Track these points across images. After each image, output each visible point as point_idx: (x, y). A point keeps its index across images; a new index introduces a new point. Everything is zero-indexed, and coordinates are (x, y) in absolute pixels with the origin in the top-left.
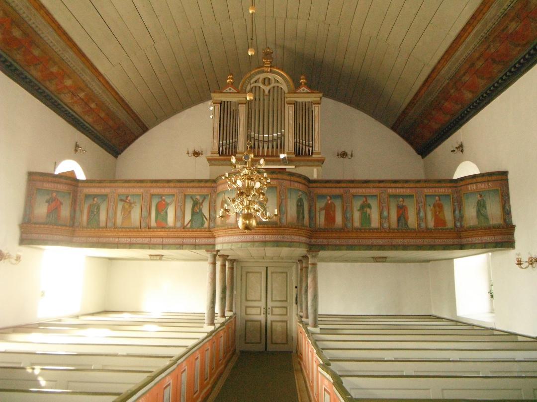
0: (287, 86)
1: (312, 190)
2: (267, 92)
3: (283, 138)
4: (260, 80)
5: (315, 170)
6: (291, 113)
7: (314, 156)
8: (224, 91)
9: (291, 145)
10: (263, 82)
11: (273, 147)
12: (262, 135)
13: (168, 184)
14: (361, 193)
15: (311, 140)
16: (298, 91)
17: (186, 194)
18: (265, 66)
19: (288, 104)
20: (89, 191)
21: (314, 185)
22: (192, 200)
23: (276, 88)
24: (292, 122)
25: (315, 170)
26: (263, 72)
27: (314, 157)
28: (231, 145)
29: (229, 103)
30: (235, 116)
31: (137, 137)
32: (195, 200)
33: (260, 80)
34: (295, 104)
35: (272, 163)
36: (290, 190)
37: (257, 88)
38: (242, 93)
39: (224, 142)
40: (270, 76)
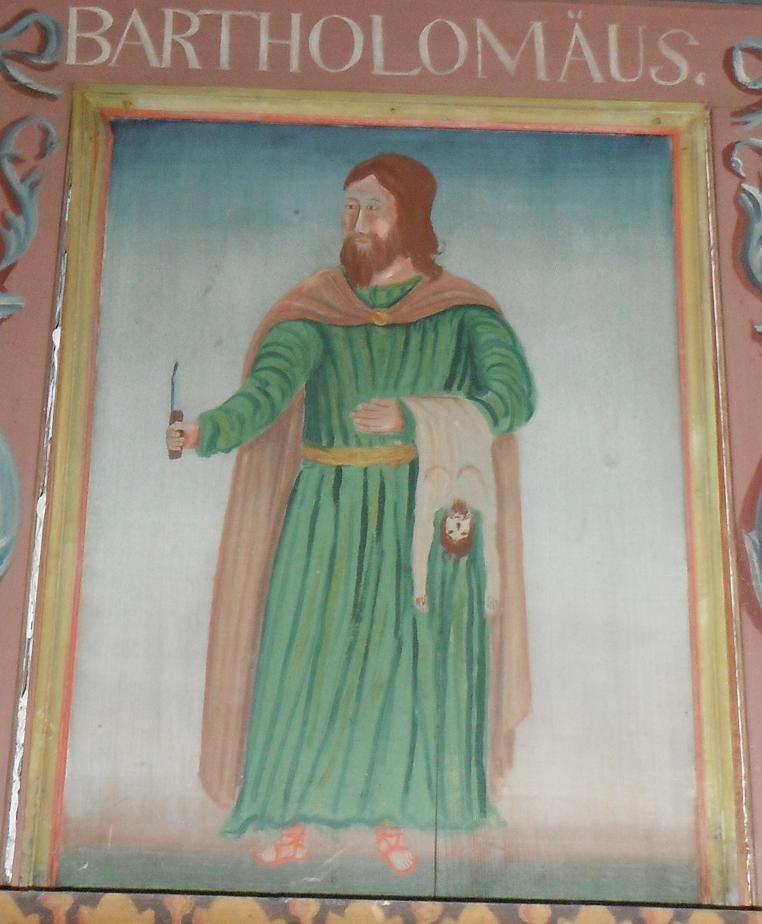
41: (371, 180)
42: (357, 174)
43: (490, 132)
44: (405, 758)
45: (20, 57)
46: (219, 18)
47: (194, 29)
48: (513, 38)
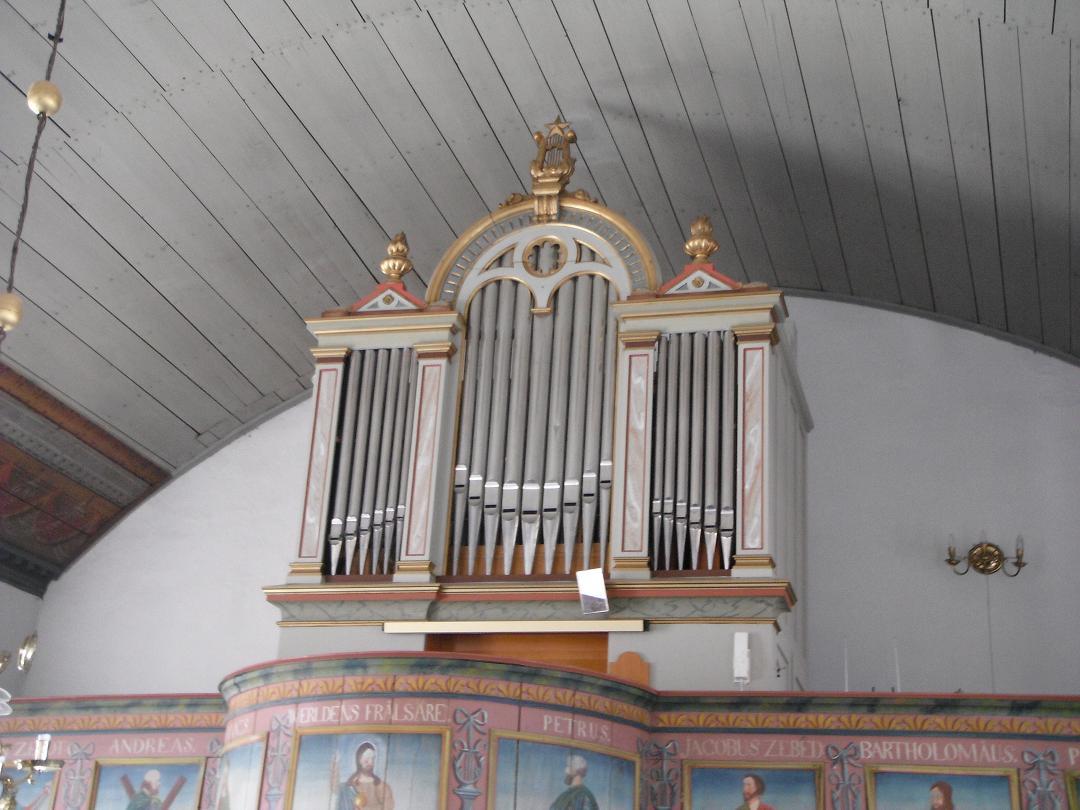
0: (629, 269)
1: (667, 742)
2: (542, 302)
3: (604, 494)
4: (518, 256)
5: (741, 639)
6: (642, 383)
7: (736, 572)
8: (364, 309)
9: (638, 526)
10: (531, 260)
11: (560, 539)
12: (536, 487)
13: (36, 718)
14: (920, 763)
15: (726, 501)
16: (673, 291)
17: (102, 761)
18: (537, 192)
19: (630, 345)
20: (339, 714)
21: (680, 718)
22: (123, 792)
23: (583, 284)
24: (641, 423)
25: (741, 639)
26: (531, 219)
27: (739, 580)
28: (377, 531)
29: (382, 356)
30: (402, 400)
31: (123, 510)
32: (137, 789)
33: (518, 256)
34: (659, 340)
35: (470, 611)
36: (517, 749)
37: (506, 289)
38: (433, 312)
39: (352, 519)
40: (555, 232)
41: (936, 789)
42: (933, 788)
43: (61, 404)
44: (662, 172)
45: (851, 756)
46: (499, 738)
47: (891, 748)
48: (968, 749)
